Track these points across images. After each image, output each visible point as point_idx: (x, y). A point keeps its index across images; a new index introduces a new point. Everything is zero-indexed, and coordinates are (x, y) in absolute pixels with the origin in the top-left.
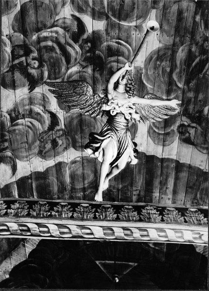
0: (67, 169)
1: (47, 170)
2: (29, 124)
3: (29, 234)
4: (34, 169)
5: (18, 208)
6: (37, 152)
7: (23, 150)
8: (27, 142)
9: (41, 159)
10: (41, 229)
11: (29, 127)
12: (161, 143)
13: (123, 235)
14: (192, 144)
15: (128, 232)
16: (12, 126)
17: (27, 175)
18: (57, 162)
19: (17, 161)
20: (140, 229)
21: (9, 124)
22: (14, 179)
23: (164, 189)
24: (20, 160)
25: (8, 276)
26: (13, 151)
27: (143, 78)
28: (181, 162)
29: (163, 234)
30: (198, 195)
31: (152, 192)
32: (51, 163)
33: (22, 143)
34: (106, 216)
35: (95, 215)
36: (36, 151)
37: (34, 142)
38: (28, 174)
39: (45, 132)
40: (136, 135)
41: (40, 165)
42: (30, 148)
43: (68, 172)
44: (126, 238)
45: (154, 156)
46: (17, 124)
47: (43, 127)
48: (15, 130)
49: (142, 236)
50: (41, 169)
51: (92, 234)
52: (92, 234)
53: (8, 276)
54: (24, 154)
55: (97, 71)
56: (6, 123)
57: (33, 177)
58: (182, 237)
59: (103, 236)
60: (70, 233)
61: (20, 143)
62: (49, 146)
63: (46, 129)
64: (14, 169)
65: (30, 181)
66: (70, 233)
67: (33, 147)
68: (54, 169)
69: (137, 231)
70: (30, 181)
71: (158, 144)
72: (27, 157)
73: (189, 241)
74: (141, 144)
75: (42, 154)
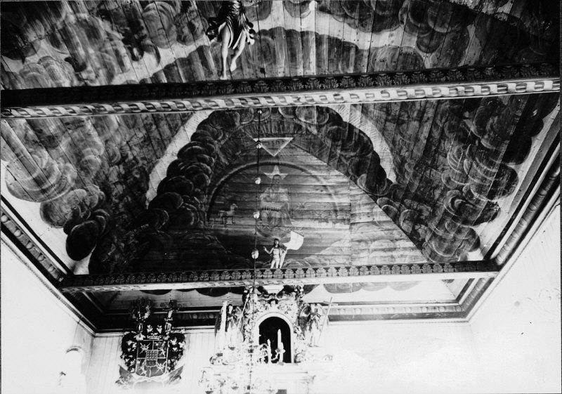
0: (210, 52)
1: (190, 54)
2: (161, 8)
3: (170, 110)
4: (177, 54)
5: (158, 91)
6: (176, 38)
7: (162, 37)
8: (164, 28)
9: (181, 45)
10: (178, 105)
11: (161, 11)
12: (298, 15)
13: (240, 104)
14: (329, 12)
15: (243, 101)
16: (145, 11)
17: (171, 62)
18: (198, 46)
19: (159, 49)
20: (252, 98)
21: (141, 10)
22: (160, 68)
23: (307, 64)
24: (161, 48)
25: (176, 158)
26: (151, 38)
27: (172, 9)
28: (320, 34)
29: (270, 100)
30: (340, 67)
31: (296, 68)
32: (192, 48)
33: (159, 29)
34: (226, 91)
35: (218, 91)
36: (175, 36)
37: (170, 26)
38: (172, 61)
39: (179, 15)
40: (272, 9)
41: (182, 51)
42: (167, 36)
43: (210, 55)
44: (243, 106)
45: (294, 30)
46: (149, 9)
47: (175, 10)
48: (148, 16)
49: (255, 104)
50: (184, 55)
51: (217, 105)
52: (217, 105)
53: (176, 158)
54: (164, 41)
55: (26, 130)
56: (137, 9)
57: (178, 63)
58: (285, 102)
59: (226, 106)
60: (201, 106)
61: (156, 29)
62: (186, 31)
63: (179, 11)
64: (158, 56)
65: (176, 68)
66: (201, 106)
67: (170, 33)
68: (197, 54)
69: (251, 100)
70: (176, 68)
71: (295, 16)
72: (167, 44)
73: (291, 104)
74: (278, 18)
75: (182, 40)
